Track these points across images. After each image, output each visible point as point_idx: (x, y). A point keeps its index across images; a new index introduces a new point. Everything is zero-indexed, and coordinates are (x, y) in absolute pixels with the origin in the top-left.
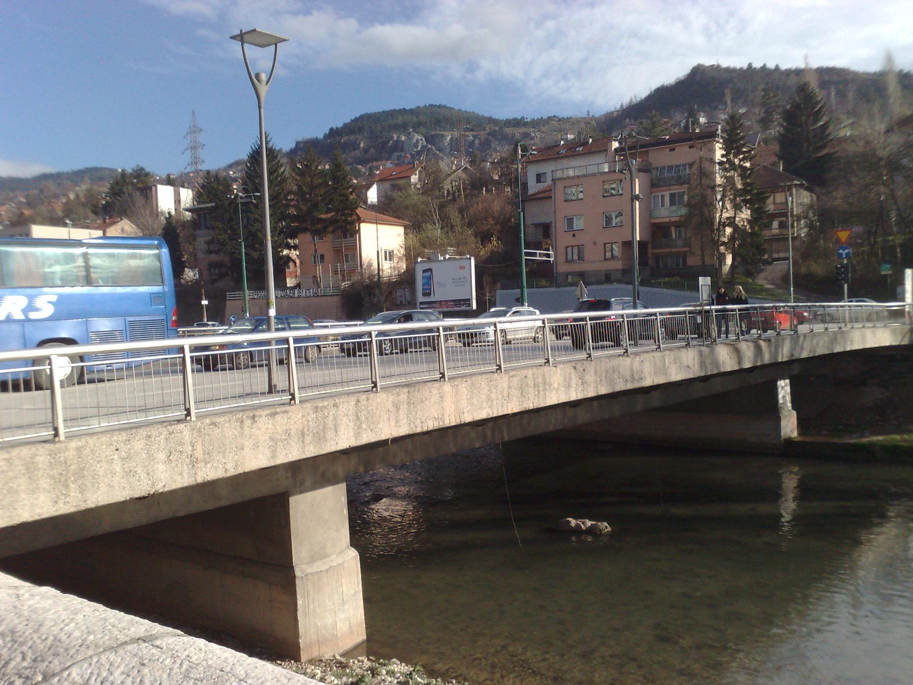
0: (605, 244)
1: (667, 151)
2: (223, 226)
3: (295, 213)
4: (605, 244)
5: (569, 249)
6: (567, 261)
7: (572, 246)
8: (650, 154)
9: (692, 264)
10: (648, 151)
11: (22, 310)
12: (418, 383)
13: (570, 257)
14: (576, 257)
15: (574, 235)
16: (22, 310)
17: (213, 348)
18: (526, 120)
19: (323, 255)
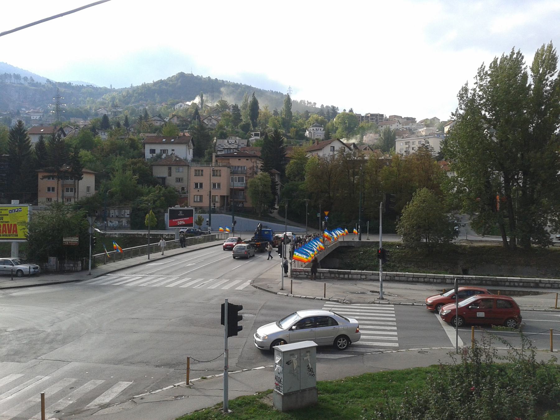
0: (194, 196)
1: (238, 160)
2: (530, 72)
3: (494, 139)
4: (194, 196)
5: (196, 197)
6: (194, 202)
7: (197, 195)
8: (230, 160)
9: (246, 206)
10: (229, 159)
11: (155, 150)
12: (216, 256)
13: (196, 200)
14: (198, 200)
15: (198, 191)
16: (155, 150)
17: (439, 281)
18: (72, 85)
19: (202, 184)
